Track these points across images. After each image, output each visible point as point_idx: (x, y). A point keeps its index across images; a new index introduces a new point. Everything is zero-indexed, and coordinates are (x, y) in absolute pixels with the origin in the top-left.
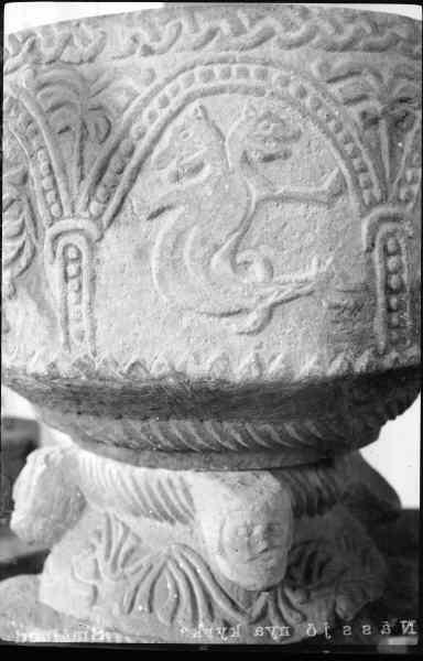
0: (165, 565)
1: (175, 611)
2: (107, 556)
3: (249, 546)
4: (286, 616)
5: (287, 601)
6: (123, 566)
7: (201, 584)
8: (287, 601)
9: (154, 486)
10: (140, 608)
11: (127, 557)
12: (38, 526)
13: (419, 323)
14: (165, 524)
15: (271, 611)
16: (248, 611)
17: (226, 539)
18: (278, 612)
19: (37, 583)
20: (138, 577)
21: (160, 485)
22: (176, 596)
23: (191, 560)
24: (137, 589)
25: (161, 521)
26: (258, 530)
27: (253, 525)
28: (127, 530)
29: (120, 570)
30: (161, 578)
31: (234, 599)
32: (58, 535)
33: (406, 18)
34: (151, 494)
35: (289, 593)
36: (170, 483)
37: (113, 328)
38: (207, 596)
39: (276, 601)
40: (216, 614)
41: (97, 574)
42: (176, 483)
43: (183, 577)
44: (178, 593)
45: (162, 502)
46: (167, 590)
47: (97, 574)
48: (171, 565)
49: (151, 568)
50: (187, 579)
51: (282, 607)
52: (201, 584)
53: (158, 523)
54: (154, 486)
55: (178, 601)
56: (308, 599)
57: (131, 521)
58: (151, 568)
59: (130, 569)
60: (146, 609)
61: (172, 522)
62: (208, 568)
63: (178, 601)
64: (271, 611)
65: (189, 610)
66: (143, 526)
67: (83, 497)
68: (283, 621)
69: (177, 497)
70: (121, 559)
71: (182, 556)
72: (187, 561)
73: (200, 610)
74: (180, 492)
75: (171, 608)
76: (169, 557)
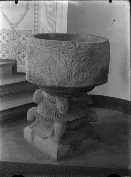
0: (52, 109)
2: (45, 107)
3: (62, 109)
7: (57, 112)
11: (47, 108)
12: (37, 101)
15: (66, 117)
18: (67, 117)
19: (36, 108)
20: (49, 110)
26: (63, 107)
28: (48, 103)
32: (39, 102)
35: (69, 115)
37: (40, 74)
41: (43, 109)
47: (43, 109)
51: (68, 117)
52: (57, 112)
55: (53, 114)
56: (72, 116)
57: (49, 103)
63: (53, 114)
64: (66, 117)
66: (50, 103)
67: (46, 4)
68: (67, 118)
76: (53, 108)
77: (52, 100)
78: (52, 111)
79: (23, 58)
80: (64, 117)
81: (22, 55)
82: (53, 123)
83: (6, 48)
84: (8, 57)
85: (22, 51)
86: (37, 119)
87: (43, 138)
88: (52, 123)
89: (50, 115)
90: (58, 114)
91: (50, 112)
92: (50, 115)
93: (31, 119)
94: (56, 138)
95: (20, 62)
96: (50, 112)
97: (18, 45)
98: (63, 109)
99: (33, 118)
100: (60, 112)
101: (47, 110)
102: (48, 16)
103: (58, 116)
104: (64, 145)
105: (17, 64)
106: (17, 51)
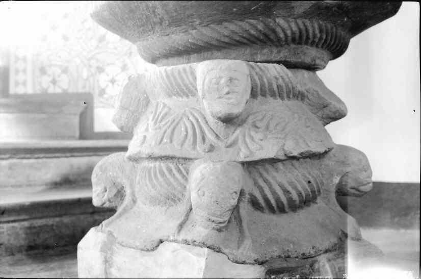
0: (182, 118)
1: (184, 141)
4: (250, 145)
5: (252, 138)
6: (160, 122)
8: (252, 138)
9: (176, 74)
10: (165, 141)
11: (163, 118)
13: (280, 3)
14: (185, 99)
15: (240, 141)
16: (226, 140)
17: (206, 87)
20: (166, 127)
21: (179, 73)
22: (185, 133)
23: (196, 115)
24: (165, 132)
25: (182, 97)
26: (223, 81)
27: (221, 77)
29: (158, 124)
30: (179, 125)
31: (218, 133)
33: (340, 118)
34: (174, 77)
35: (253, 133)
36: (185, 70)
38: (202, 132)
39: (244, 136)
40: (207, 141)
42: (188, 69)
43: (191, 126)
44: (187, 132)
45: (179, 80)
46: (181, 131)
48: (185, 119)
49: (174, 120)
50: (193, 125)
51: (247, 140)
52: (197, 121)
53: (180, 99)
54: (176, 74)
55: (186, 135)
58: (174, 120)
59: (163, 123)
60: (169, 141)
61: (187, 96)
62: (205, 118)
63: (186, 135)
65: (192, 139)
67: (147, 98)
69: (188, 78)
70: (159, 119)
71: (191, 113)
72: (194, 116)
73: (198, 140)
74: (189, 74)
75: (182, 139)
76: (184, 114)
77: (179, 80)
78: (181, 123)
79: (110, 84)
80: (229, 142)
81: (108, 75)
82: (186, 180)
83: (60, 57)
84: (65, 87)
85: (108, 65)
86: (128, 191)
87: (148, 250)
88: (184, 176)
89: (171, 141)
90: (207, 132)
91: (173, 132)
92: (171, 141)
93: (106, 197)
94: (200, 230)
95: (101, 100)
96: (173, 132)
97: (98, 46)
98: (226, 90)
99: (115, 191)
100: (212, 125)
101: (160, 128)
102: (193, 86)
103: (204, 139)
104: (237, 262)
105: (95, 105)
106: (94, 63)
